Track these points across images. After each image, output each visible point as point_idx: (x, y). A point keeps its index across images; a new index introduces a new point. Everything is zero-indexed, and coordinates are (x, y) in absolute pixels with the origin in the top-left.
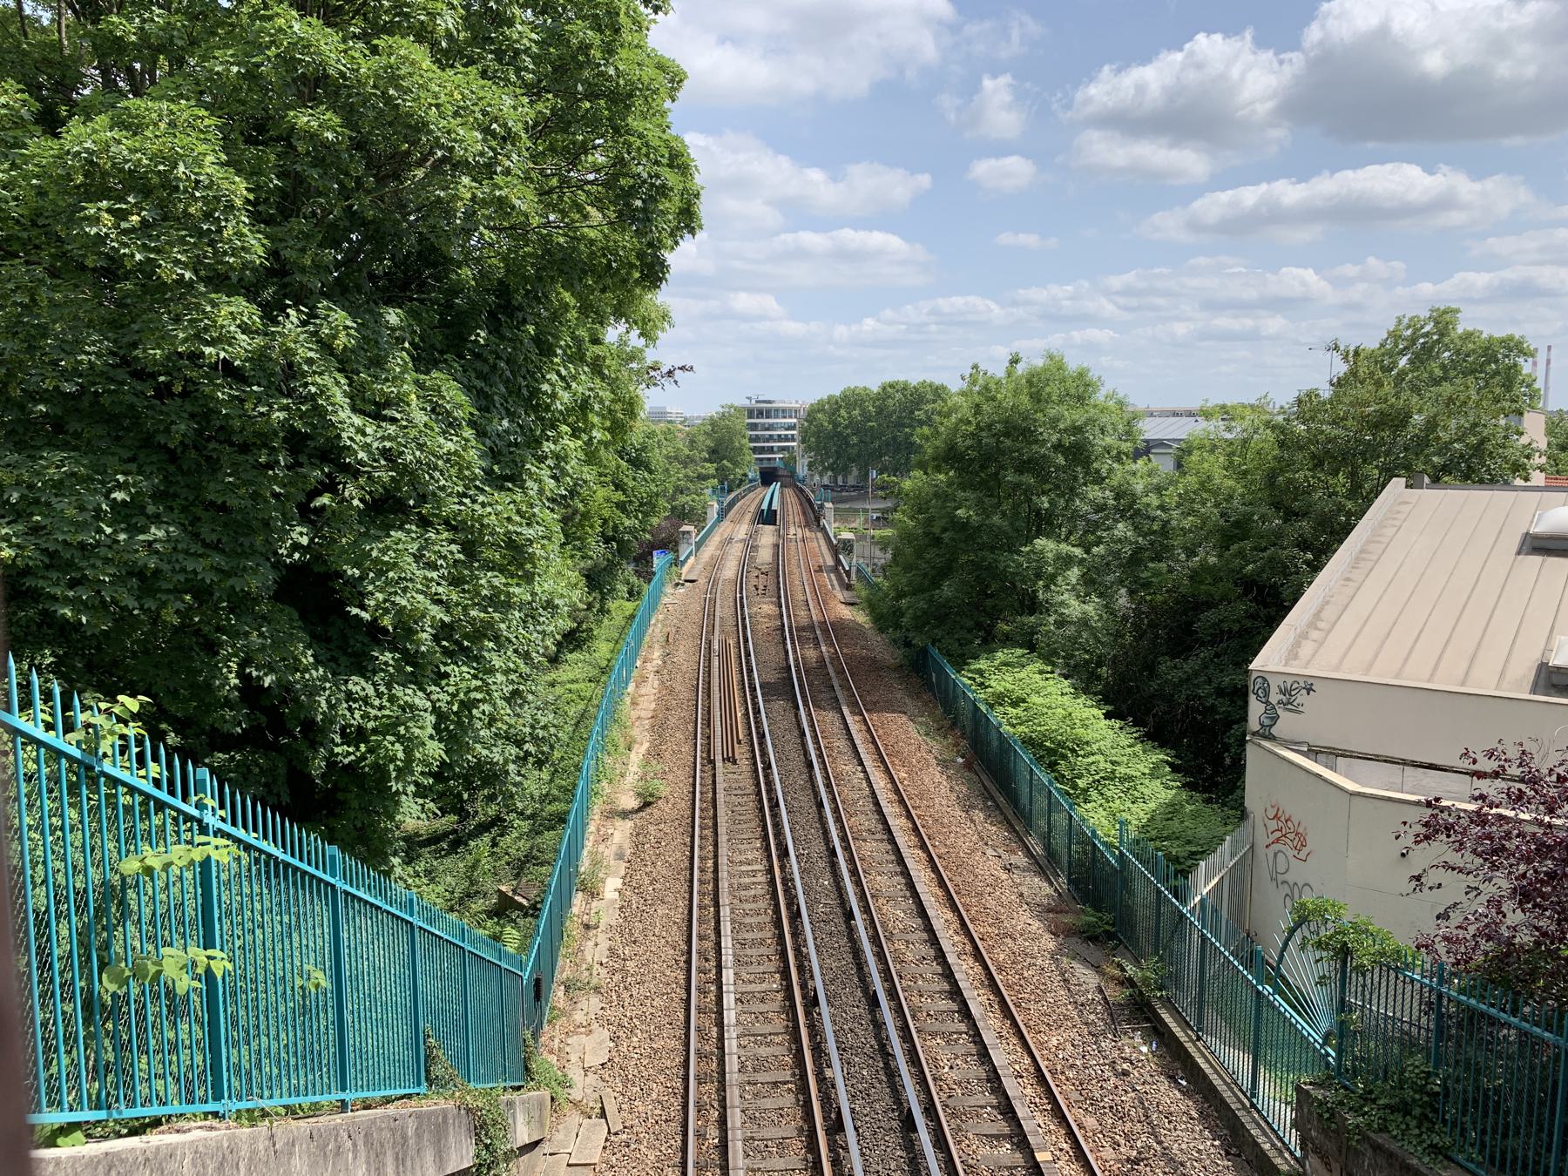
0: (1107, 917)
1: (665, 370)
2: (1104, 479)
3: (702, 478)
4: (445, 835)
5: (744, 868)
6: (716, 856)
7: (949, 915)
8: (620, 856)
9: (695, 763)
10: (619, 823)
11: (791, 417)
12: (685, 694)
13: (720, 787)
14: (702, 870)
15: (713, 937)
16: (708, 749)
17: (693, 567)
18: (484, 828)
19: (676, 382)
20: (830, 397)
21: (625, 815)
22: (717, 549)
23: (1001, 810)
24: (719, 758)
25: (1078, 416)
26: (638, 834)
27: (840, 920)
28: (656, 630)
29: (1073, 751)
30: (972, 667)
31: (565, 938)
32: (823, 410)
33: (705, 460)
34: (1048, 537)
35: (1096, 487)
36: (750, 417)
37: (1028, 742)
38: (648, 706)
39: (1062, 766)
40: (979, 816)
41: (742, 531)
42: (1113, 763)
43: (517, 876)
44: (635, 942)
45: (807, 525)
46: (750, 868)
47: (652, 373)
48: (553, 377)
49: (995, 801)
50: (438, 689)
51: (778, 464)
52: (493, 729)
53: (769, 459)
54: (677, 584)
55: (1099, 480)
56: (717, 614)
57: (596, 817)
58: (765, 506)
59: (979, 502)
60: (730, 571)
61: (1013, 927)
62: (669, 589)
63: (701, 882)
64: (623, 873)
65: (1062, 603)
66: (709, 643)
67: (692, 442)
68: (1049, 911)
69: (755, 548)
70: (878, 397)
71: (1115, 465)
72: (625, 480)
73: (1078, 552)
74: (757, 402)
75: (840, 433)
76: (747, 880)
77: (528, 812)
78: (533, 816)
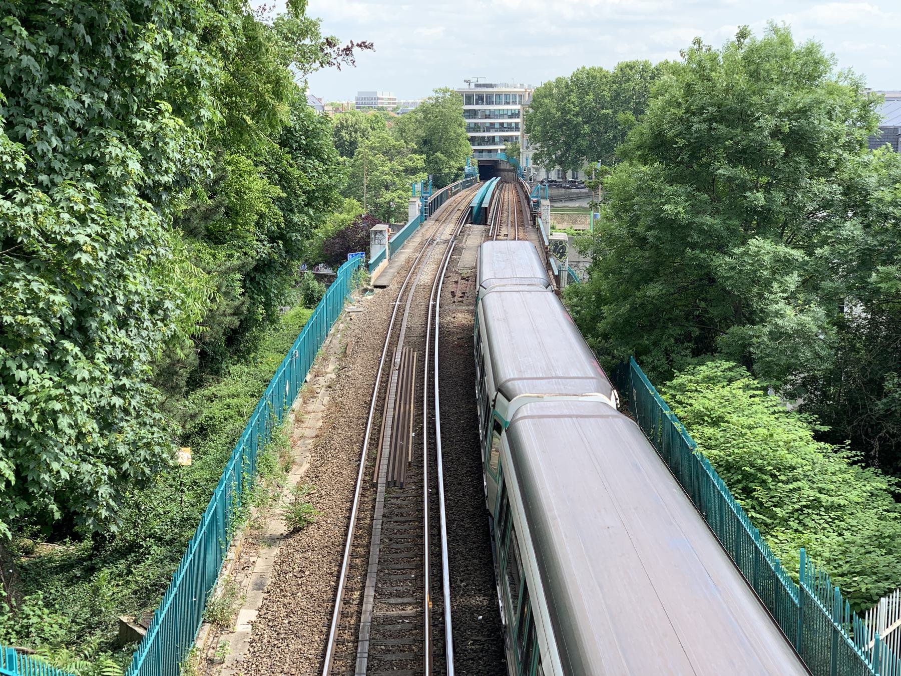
1: (343, 46)
2: (832, 170)
3: (412, 171)
4: (80, 560)
6: (363, 587)
8: (259, 586)
9: (355, 487)
10: (264, 550)
11: (514, 103)
12: (354, 411)
13: (379, 512)
14: (346, 602)
16: (371, 471)
17: (385, 271)
18: (121, 553)
20: (558, 81)
21: (273, 541)
22: (416, 251)
24: (382, 481)
25: (803, 98)
28: (335, 338)
29: (774, 476)
32: (551, 95)
33: (414, 152)
34: (765, 237)
35: (822, 180)
38: (314, 423)
39: (760, 493)
41: (447, 231)
45: (521, 224)
47: (328, 50)
50: (15, 399)
51: (499, 156)
52: (80, 447)
53: (490, 151)
54: (366, 290)
55: (827, 172)
56: (404, 323)
57: (237, 543)
58: (475, 204)
59: (690, 197)
60: (426, 275)
62: (355, 296)
63: (343, 615)
64: (260, 604)
65: (777, 314)
66: (390, 355)
67: (402, 131)
69: (457, 250)
71: (846, 155)
72: (290, 169)
73: (798, 254)
74: (477, 86)
75: (569, 121)
77: (167, 537)
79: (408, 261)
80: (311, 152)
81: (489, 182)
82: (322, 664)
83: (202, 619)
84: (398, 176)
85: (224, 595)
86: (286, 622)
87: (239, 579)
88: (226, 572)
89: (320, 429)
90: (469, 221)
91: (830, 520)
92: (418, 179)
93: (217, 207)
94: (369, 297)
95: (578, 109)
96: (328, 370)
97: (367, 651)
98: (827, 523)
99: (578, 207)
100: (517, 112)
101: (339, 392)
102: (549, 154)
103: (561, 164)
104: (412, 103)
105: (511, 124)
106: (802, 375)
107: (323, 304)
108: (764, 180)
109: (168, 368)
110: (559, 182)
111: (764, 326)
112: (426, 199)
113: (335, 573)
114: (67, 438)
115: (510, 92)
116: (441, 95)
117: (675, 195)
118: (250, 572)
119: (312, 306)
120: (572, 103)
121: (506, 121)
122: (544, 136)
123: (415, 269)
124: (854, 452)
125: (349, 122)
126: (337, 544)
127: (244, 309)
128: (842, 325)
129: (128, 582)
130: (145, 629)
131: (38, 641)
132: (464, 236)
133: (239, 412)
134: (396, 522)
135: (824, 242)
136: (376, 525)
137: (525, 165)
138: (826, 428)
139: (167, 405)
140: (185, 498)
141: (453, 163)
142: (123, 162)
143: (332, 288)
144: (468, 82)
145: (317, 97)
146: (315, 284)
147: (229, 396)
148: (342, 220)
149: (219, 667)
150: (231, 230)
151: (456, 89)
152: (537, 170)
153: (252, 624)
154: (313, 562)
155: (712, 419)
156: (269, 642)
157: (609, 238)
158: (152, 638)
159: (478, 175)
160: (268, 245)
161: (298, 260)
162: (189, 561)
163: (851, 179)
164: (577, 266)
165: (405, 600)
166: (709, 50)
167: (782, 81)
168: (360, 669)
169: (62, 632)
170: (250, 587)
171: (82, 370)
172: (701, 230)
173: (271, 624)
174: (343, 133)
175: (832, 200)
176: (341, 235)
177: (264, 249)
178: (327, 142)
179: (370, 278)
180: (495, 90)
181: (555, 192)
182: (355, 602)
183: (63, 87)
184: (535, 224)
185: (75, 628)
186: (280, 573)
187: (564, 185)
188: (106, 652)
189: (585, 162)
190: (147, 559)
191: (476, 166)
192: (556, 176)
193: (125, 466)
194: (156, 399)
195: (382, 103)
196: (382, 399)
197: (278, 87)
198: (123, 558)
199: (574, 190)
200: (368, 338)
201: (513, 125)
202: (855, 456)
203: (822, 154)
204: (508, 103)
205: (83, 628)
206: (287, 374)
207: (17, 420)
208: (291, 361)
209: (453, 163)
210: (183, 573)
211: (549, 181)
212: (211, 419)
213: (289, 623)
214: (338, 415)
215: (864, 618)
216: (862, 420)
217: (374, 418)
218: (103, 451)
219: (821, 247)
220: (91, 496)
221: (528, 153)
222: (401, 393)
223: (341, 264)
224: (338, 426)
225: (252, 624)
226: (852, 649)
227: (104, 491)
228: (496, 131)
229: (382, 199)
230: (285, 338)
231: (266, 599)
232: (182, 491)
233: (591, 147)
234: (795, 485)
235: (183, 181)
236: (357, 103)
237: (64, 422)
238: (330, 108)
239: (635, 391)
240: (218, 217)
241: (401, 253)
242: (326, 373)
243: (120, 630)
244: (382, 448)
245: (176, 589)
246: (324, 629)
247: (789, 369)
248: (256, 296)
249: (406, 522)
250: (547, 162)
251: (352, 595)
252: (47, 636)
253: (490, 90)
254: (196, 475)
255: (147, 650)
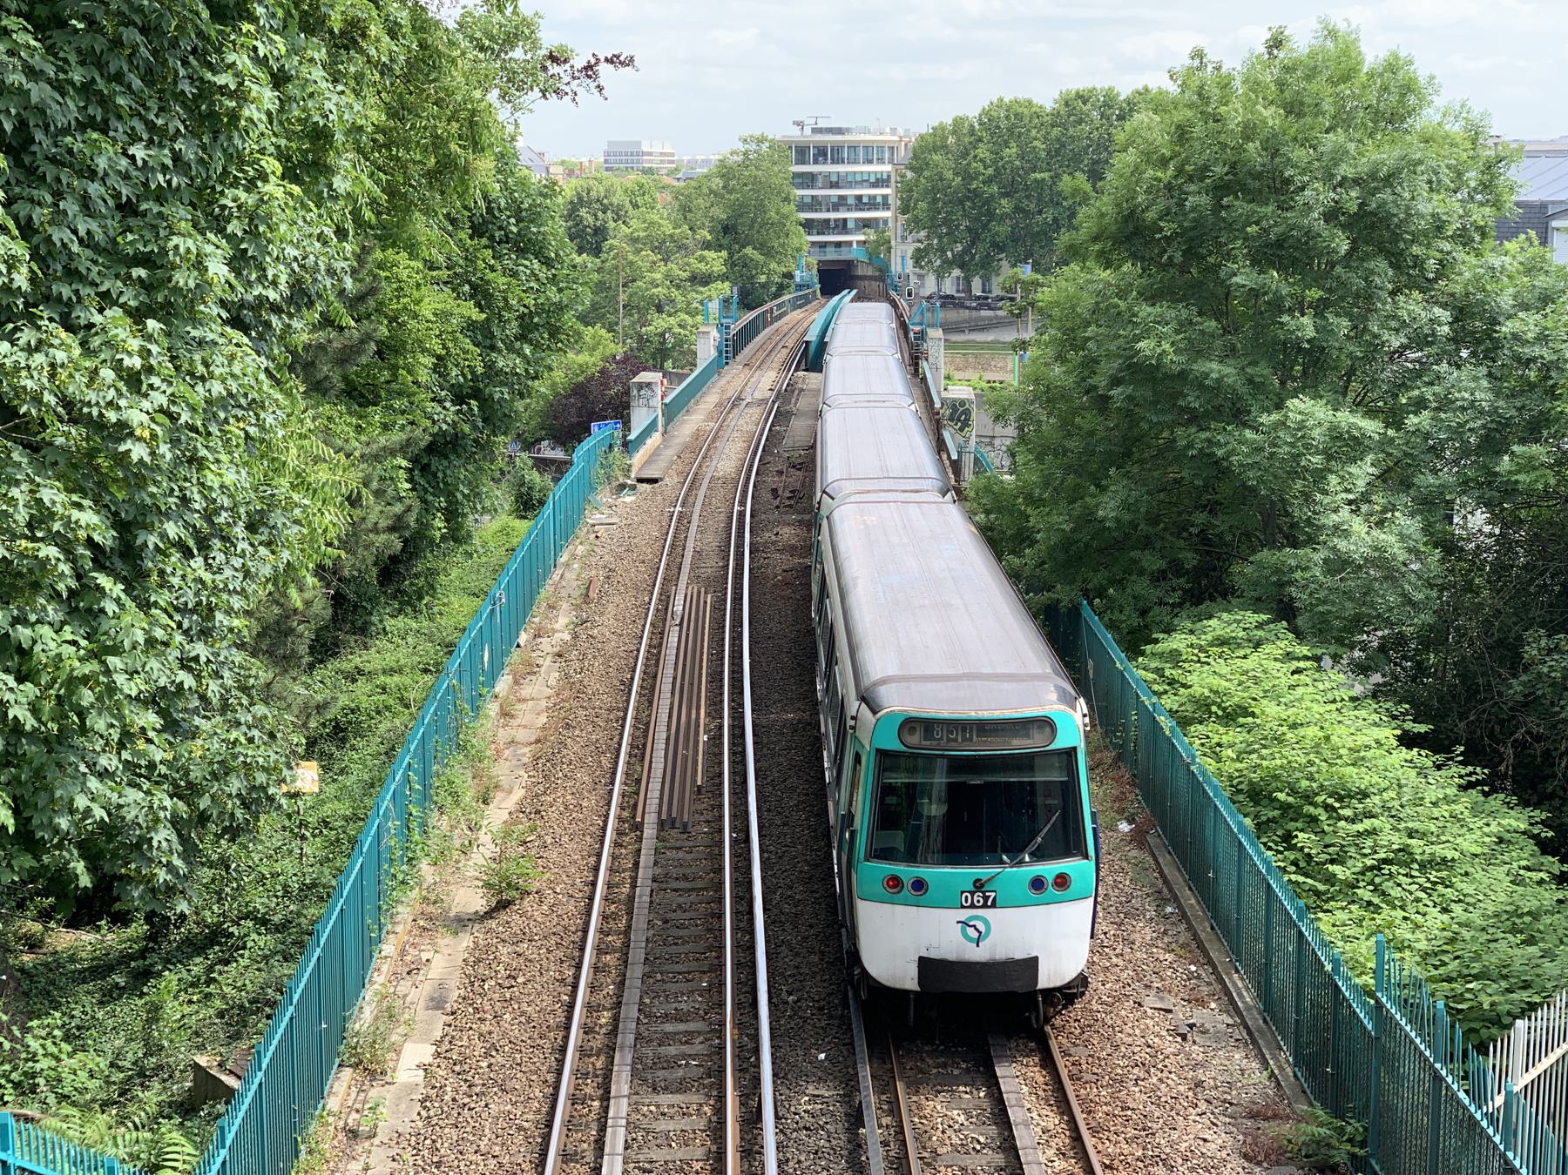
0: (1354, 1127)
1: (579, 63)
4: (125, 959)
5: (669, 1027)
7: (1053, 1120)
8: (437, 1003)
10: (445, 940)
11: (881, 161)
15: (590, 1157)
16: (631, 802)
17: (656, 453)
18: (194, 946)
19: (600, 88)
20: (958, 122)
21: (462, 923)
22: (710, 418)
23: (1189, 923)
25: (1380, 154)
26: (479, 961)
27: (838, 1128)
30: (1159, 647)
31: (303, 1156)
32: (944, 147)
33: (707, 246)
34: (1317, 396)
35: (1416, 294)
36: (801, 160)
37: (1255, 794)
38: (532, 718)
40: (1144, 932)
42: (1411, 834)
43: (235, 1037)
44: (438, 1165)
46: (682, 1027)
47: (554, 69)
48: (243, 61)
49: (1180, 907)
51: (855, 253)
52: (126, 755)
53: (838, 244)
56: (690, 544)
57: (399, 929)
59: (1182, 326)
60: (728, 459)
61: (1171, 1144)
62: (604, 496)
64: (438, 1034)
66: (666, 599)
67: (685, 209)
68: (1253, 1116)
70: (1057, 120)
71: (1460, 254)
72: (490, 276)
74: (815, 131)
75: (976, 194)
76: (672, 1050)
77: (277, 919)
78: (282, 928)
79: (697, 435)
80: (526, 246)
81: (836, 298)
82: (547, 1138)
83: (337, 1061)
84: (678, 287)
85: (376, 1018)
86: (484, 1064)
87: (401, 990)
88: (379, 979)
89: (544, 728)
90: (803, 366)
91: (1429, 885)
92: (714, 294)
93: (362, 342)
94: (628, 499)
95: (990, 171)
96: (557, 626)
97: (624, 1115)
98: (1424, 890)
99: (992, 342)
100: (885, 177)
101: (577, 665)
102: (942, 250)
103: (962, 267)
104: (703, 161)
105: (875, 197)
106: (1379, 633)
107: (548, 510)
108: (1314, 294)
109: (277, 623)
110: (960, 298)
111: (1314, 549)
112: (728, 327)
113: (570, 980)
114: (102, 742)
115: (873, 142)
116: (754, 147)
117: (1159, 323)
118: (421, 977)
119: (529, 514)
120: (981, 160)
121: (866, 192)
122: (933, 219)
123: (708, 450)
124: (1470, 769)
125: (593, 194)
126: (573, 929)
127: (411, 519)
128: (1450, 547)
129: (208, 996)
130: (239, 1078)
131: (51, 1100)
132: (793, 392)
133: (401, 699)
134: (676, 890)
135: (1420, 405)
136: (640, 896)
137: (899, 269)
138: (1422, 728)
139: (276, 688)
140: (308, 850)
141: (773, 265)
142: (199, 265)
143: (563, 484)
144: (800, 124)
145: (537, 150)
146: (534, 477)
147: (384, 672)
148: (581, 366)
149: (367, 1144)
150: (388, 382)
151: (778, 138)
152: (921, 277)
153: (425, 1068)
154: (530, 961)
155: (1224, 709)
156: (454, 1100)
157: (1049, 396)
158: (251, 1094)
159: (819, 286)
160: (453, 409)
161: (505, 434)
162: (314, 959)
163: (1467, 294)
164: (991, 444)
165: (691, 1026)
166: (1218, 69)
167: (1342, 120)
168: (613, 1146)
169: (93, 1084)
170: (422, 1004)
171: (132, 626)
172: (1200, 384)
173: (457, 1068)
174: (583, 212)
175: (1433, 335)
176: (579, 390)
177: (447, 415)
178: (555, 229)
179: (630, 466)
180: (847, 137)
181: (953, 315)
182: (604, 1031)
183: (95, 136)
184: (916, 371)
185: (118, 1077)
186: (474, 982)
187: (968, 303)
188: (170, 1118)
189: (1004, 263)
190: (242, 956)
191: (815, 271)
192: (954, 289)
193: (204, 803)
194: (256, 678)
195: (651, 161)
196: (651, 676)
197: (474, 130)
198: (199, 955)
199: (985, 313)
200: (627, 571)
201: (879, 200)
202: (1470, 774)
203: (1416, 250)
204: (870, 162)
205: (131, 1077)
206: (486, 634)
207: (15, 717)
208: (492, 611)
209: (773, 265)
210: (304, 980)
211: (941, 297)
212: (353, 711)
213: (490, 1066)
214: (574, 704)
215: (1488, 1055)
216: (1484, 711)
217: (637, 709)
218: (163, 769)
219: (1416, 413)
220: (138, 846)
221: (904, 247)
222: (684, 665)
223: (580, 442)
224: (574, 724)
225: (425, 1068)
226: (1465, 1108)
227: (163, 836)
228: (848, 210)
229: (651, 328)
230: (483, 570)
231: (450, 1025)
232: (303, 838)
233: (1015, 239)
234: (1367, 824)
235: (300, 296)
236: (606, 161)
237: (99, 723)
238: (560, 169)
239: (1091, 663)
240: (364, 360)
241: (684, 422)
242: (554, 631)
243: (194, 1080)
244: (651, 762)
245: (291, 1009)
246: (551, 1078)
247: (1358, 623)
248: (430, 498)
249: (693, 889)
250: (938, 262)
251: (598, 1018)
252: (66, 1091)
253: (839, 138)
254: (327, 810)
255: (241, 1115)
